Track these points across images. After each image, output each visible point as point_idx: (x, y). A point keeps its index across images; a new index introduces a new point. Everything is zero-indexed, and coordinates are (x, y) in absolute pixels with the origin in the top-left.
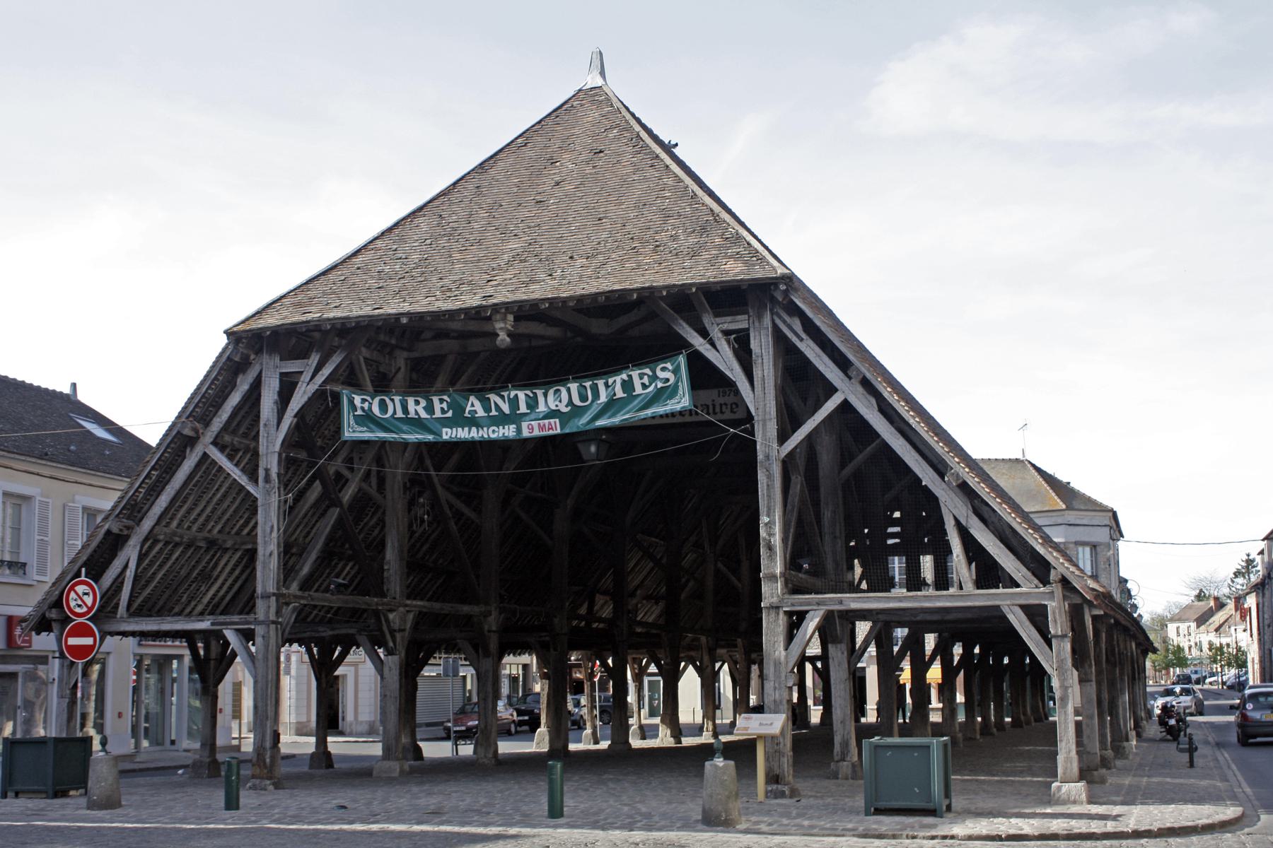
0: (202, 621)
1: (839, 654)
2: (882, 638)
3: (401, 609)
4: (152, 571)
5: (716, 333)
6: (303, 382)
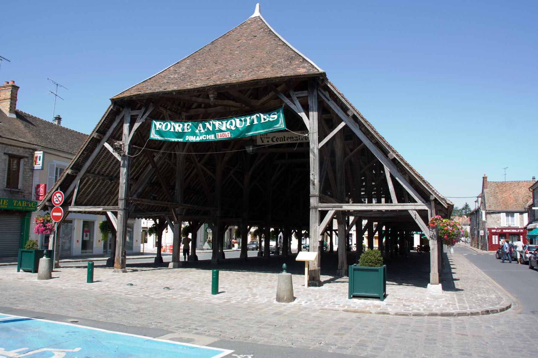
1: (342, 228)
2: (358, 223)
3: (181, 207)
4: (89, 190)
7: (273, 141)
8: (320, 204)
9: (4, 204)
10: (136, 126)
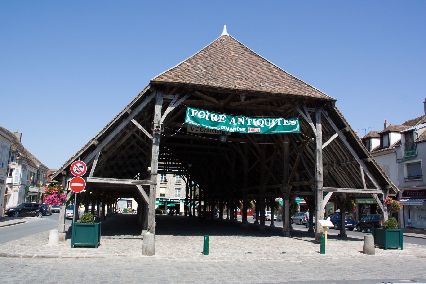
5: (307, 112)
6: (172, 102)
7: (201, 131)
8: (324, 187)
10: (170, 109)
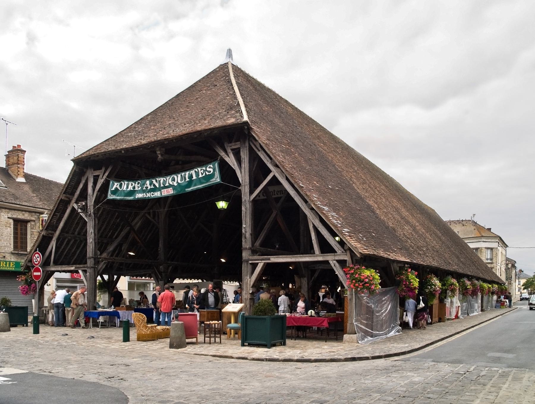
0: (72, 267)
9: (11, 266)
